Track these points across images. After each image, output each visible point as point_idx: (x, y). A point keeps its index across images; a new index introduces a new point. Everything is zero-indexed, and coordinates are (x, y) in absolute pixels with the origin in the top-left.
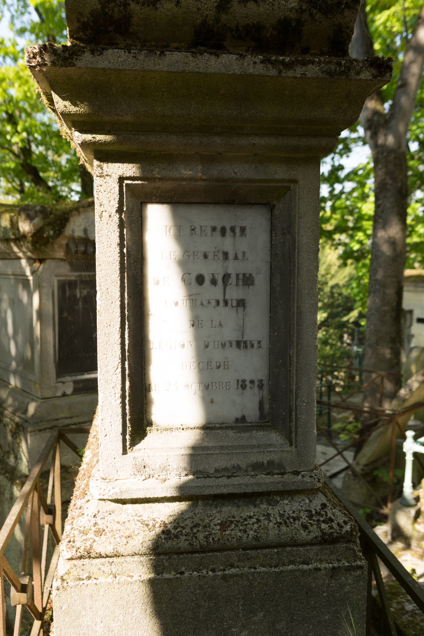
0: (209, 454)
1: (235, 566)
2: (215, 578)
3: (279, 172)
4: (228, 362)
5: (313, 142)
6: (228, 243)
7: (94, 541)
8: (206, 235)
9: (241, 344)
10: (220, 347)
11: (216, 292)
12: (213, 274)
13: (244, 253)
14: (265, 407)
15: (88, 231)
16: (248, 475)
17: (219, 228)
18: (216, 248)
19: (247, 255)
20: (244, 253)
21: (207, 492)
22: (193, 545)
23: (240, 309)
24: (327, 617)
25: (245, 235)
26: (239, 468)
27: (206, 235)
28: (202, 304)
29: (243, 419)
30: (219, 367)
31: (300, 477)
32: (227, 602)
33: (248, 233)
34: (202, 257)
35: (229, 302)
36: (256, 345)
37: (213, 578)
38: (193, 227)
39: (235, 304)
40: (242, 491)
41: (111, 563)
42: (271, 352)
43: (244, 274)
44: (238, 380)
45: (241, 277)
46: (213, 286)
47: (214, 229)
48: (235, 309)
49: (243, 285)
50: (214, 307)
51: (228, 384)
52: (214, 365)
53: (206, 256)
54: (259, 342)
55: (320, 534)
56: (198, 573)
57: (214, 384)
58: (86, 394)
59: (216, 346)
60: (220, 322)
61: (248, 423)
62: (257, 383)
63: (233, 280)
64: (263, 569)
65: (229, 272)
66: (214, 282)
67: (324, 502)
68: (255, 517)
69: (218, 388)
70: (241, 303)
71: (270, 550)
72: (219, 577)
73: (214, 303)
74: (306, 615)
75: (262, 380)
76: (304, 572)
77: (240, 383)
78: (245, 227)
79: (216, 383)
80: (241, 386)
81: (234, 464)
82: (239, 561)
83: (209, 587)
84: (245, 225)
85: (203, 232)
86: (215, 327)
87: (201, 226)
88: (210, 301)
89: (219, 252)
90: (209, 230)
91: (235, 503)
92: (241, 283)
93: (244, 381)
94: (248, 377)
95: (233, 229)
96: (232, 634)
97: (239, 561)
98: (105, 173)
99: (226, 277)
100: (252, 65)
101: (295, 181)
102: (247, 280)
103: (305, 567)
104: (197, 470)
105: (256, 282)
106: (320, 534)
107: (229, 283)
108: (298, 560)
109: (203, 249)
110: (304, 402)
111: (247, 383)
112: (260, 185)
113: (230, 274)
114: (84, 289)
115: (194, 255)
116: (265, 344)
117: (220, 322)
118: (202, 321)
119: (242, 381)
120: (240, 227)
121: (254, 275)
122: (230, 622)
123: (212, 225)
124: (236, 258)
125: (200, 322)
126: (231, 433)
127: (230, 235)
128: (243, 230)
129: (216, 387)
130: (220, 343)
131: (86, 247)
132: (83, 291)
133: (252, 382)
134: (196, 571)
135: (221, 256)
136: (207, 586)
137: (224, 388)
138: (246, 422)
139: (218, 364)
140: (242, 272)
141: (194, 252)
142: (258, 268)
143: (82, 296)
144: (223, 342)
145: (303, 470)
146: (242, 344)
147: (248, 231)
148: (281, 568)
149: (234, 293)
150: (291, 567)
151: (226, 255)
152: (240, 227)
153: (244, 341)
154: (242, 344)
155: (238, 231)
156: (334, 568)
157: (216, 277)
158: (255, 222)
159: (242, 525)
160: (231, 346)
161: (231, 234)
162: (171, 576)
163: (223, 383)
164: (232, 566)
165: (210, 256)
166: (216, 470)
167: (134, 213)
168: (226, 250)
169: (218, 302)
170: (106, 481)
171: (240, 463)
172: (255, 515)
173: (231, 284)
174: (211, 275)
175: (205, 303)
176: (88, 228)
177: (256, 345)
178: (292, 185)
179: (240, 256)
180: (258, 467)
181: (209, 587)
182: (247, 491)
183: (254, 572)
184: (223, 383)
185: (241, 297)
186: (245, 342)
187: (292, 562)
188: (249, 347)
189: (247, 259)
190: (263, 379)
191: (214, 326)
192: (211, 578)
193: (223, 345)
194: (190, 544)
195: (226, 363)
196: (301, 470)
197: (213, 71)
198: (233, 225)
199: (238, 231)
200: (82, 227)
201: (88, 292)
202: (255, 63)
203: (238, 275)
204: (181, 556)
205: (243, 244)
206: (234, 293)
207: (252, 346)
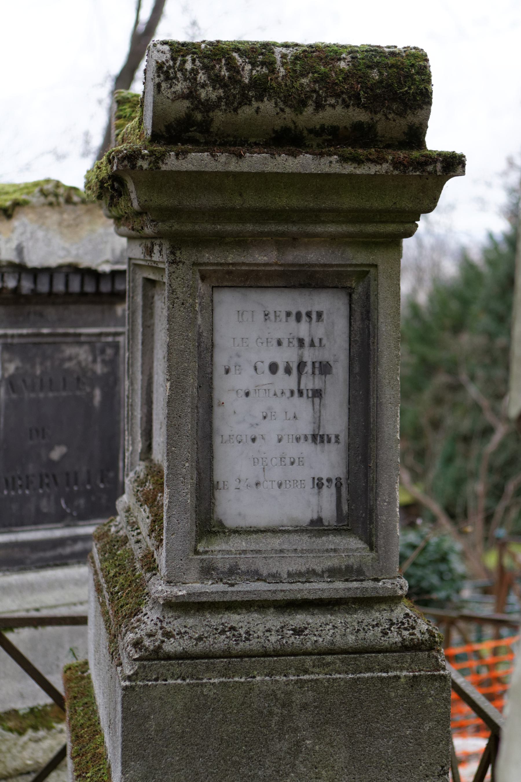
0: (283, 557)
1: (309, 672)
2: (287, 684)
3: (360, 257)
4: (303, 458)
5: (391, 228)
6: (303, 330)
7: (163, 642)
8: (280, 321)
9: (318, 438)
10: (295, 441)
11: (291, 382)
12: (287, 362)
13: (321, 340)
14: (343, 508)
15: (25, 251)
16: (324, 582)
17: (294, 313)
18: (291, 334)
19: (324, 342)
20: (321, 340)
21: (280, 596)
22: (265, 647)
23: (317, 400)
24: (408, 732)
25: (322, 321)
26: (314, 572)
27: (280, 321)
28: (275, 395)
29: (320, 520)
30: (292, 463)
31: (380, 584)
32: (301, 710)
33: (325, 319)
34: (275, 343)
35: (305, 392)
36: (333, 439)
37: (286, 683)
38: (266, 312)
39: (310, 395)
40: (317, 597)
41: (180, 665)
42: (349, 447)
43: (320, 363)
44: (314, 478)
45: (317, 365)
46: (287, 375)
47: (288, 314)
48: (310, 399)
49: (320, 374)
50: (288, 398)
51: (303, 482)
52: (288, 461)
53: (279, 343)
54: (337, 437)
55: (400, 639)
56: (271, 677)
57: (288, 482)
58: (8, 573)
59: (291, 440)
60: (295, 414)
61: (325, 526)
62: (334, 482)
63: (309, 368)
64: (338, 676)
65: (305, 360)
66: (288, 371)
67: (407, 612)
68: (331, 624)
69: (292, 487)
70: (317, 394)
71: (347, 656)
72: (293, 683)
73: (288, 394)
74: (386, 729)
75: (340, 479)
76: (382, 679)
77: (316, 481)
78: (322, 311)
79: (290, 481)
80: (317, 484)
81: (308, 569)
82: (314, 666)
83: (282, 693)
84: (322, 310)
85: (278, 318)
86: (289, 419)
87: (275, 312)
88: (285, 391)
89: (293, 339)
90: (283, 316)
91: (310, 611)
92: (317, 371)
93: (320, 479)
94: (325, 476)
95: (309, 315)
96: (306, 746)
97: (314, 666)
98: (178, 259)
99: (301, 365)
100: (330, 165)
101: (376, 266)
102: (324, 368)
103: (384, 675)
104: (269, 574)
105: (334, 370)
106: (400, 639)
107: (305, 372)
108: (377, 667)
109: (279, 335)
110: (386, 502)
111: (324, 481)
112: (337, 269)
113: (306, 362)
114: (10, 361)
115: (267, 342)
116: (343, 438)
117: (295, 414)
118: (275, 412)
119: (318, 479)
120: (317, 312)
121: (331, 363)
122: (304, 733)
123: (287, 310)
124: (312, 344)
125: (273, 414)
126: (305, 538)
127: (306, 321)
128: (320, 315)
129: (290, 485)
130: (294, 436)
131: (19, 281)
132: (7, 365)
133: (329, 480)
134: (268, 676)
135: (295, 343)
136: (280, 692)
137: (299, 487)
138: (323, 525)
139: (292, 460)
140: (320, 359)
141: (267, 339)
142: (335, 355)
143: (6, 375)
144: (298, 436)
145: (385, 577)
146: (318, 438)
147: (325, 316)
148: (358, 675)
149: (309, 383)
150: (367, 675)
151: (301, 342)
152: (317, 312)
153: (320, 435)
154: (318, 438)
155: (314, 316)
156: (414, 676)
157: (291, 365)
158: (332, 307)
159: (317, 631)
160: (306, 441)
161: (308, 319)
162: (243, 680)
163: (297, 481)
164: (306, 672)
165: (285, 343)
166: (290, 574)
167: (205, 298)
168: (301, 336)
169: (292, 393)
170: (171, 584)
171: (315, 567)
172: (332, 622)
173: (306, 373)
174: (285, 363)
175: (279, 393)
176: (25, 244)
177: (333, 439)
178: (372, 270)
179: (317, 343)
180: (334, 573)
181: (282, 693)
182: (323, 597)
183: (329, 678)
184: (297, 481)
185: (317, 387)
186: (322, 437)
187: (370, 669)
188: (325, 442)
189: (324, 346)
190: (342, 477)
191: (288, 418)
192: (284, 682)
193: (298, 439)
194: (263, 647)
195: (301, 459)
196: (383, 577)
197: (290, 171)
198: (309, 309)
199: (314, 316)
200: (14, 244)
201: (17, 369)
202: (331, 162)
203: (313, 363)
204: (253, 659)
205: (319, 331)
206: (309, 383)
207: (329, 441)
